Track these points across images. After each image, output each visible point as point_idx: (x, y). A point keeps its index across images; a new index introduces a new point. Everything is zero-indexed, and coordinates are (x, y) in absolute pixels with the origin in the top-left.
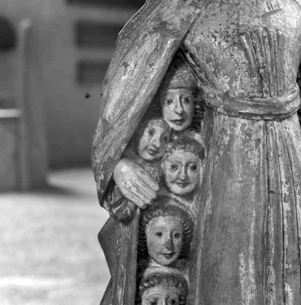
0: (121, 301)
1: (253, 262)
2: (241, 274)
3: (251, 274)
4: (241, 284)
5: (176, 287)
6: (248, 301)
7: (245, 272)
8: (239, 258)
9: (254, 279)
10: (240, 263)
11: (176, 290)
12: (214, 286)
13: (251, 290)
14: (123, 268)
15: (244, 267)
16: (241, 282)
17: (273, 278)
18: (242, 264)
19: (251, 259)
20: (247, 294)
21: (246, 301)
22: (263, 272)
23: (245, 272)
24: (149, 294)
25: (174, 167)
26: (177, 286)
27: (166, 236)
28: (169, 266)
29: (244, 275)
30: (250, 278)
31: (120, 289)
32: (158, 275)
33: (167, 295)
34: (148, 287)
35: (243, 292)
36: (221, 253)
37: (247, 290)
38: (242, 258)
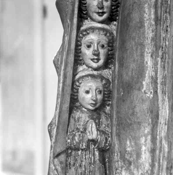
0: (67, 44)
1: (154, 10)
2: (145, 19)
3: (152, 18)
4: (145, 26)
5: (105, 36)
6: (150, 38)
7: (148, 17)
8: (144, 8)
9: (154, 22)
10: (145, 11)
11: (105, 38)
12: (127, 29)
13: (152, 30)
14: (69, 22)
15: (148, 14)
16: (146, 25)
17: (168, 22)
18: (146, 12)
19: (153, 9)
20: (149, 33)
21: (149, 38)
22: (161, 16)
23: (148, 17)
24: (86, 39)
25: (87, 92)
26: (106, 35)
27: (95, 46)
28: (102, 22)
29: (148, 20)
30: (151, 21)
31: (66, 36)
32: (93, 27)
33: (98, 40)
34: (85, 35)
35: (147, 31)
36: (133, 6)
37: (150, 30)
38: (147, 7)
